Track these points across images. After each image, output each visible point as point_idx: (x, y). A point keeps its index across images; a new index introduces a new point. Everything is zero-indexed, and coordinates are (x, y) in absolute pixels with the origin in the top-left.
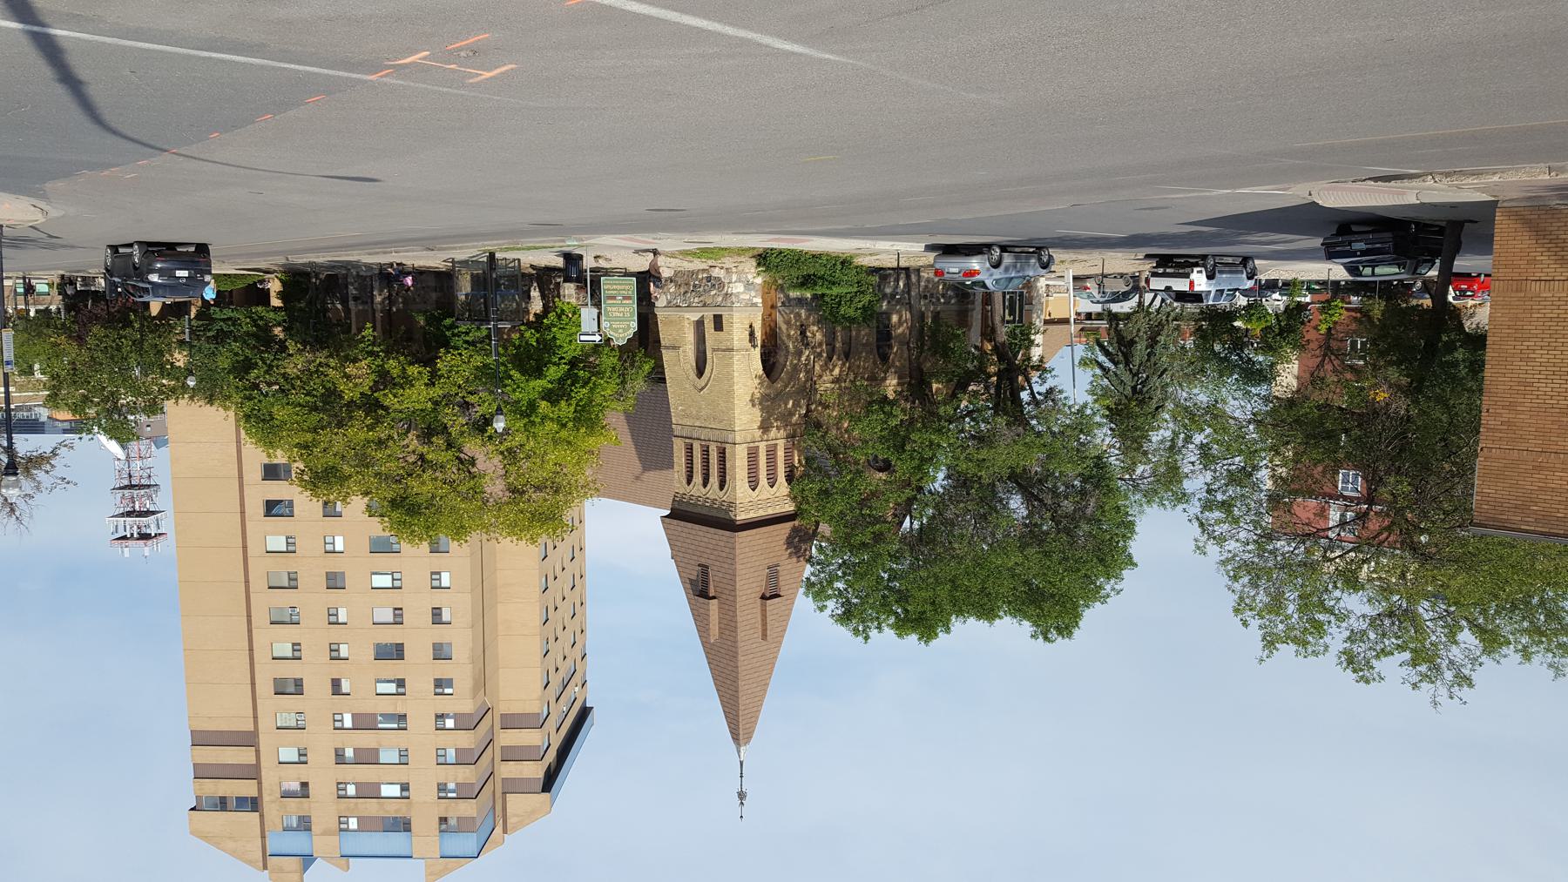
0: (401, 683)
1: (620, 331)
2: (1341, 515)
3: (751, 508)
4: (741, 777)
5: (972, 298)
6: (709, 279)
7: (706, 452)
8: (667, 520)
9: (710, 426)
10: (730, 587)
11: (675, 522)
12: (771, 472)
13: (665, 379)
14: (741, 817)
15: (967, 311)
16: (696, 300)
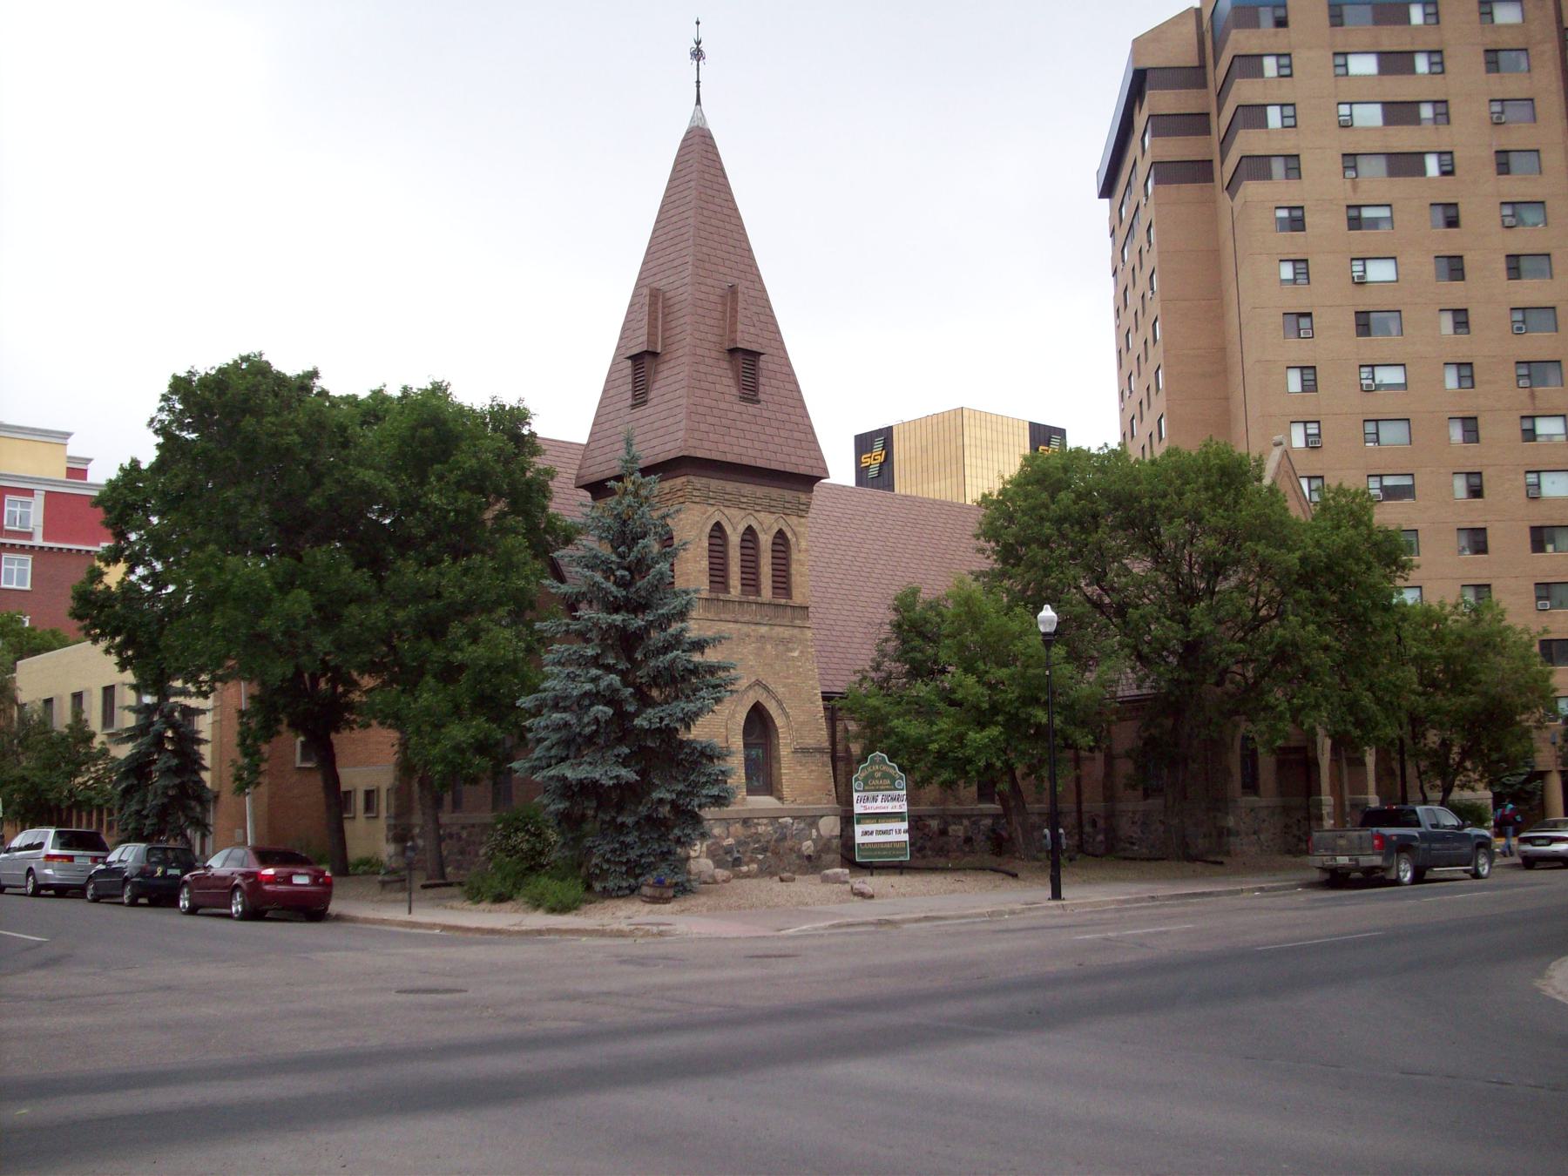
0: (1355, 223)
1: (878, 775)
2: (436, 505)
3: (668, 496)
4: (698, 82)
5: (391, 835)
6: (737, 862)
7: (751, 581)
8: (824, 475)
9: (738, 626)
10: (702, 368)
11: (803, 470)
12: (780, 555)
13: (824, 699)
14: (698, 23)
15: (398, 816)
16: (761, 829)
